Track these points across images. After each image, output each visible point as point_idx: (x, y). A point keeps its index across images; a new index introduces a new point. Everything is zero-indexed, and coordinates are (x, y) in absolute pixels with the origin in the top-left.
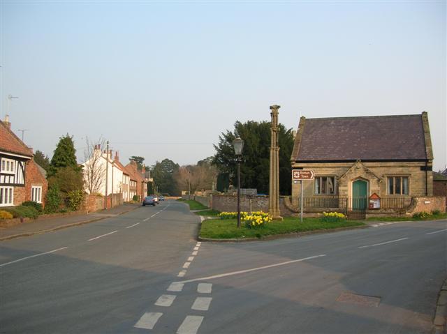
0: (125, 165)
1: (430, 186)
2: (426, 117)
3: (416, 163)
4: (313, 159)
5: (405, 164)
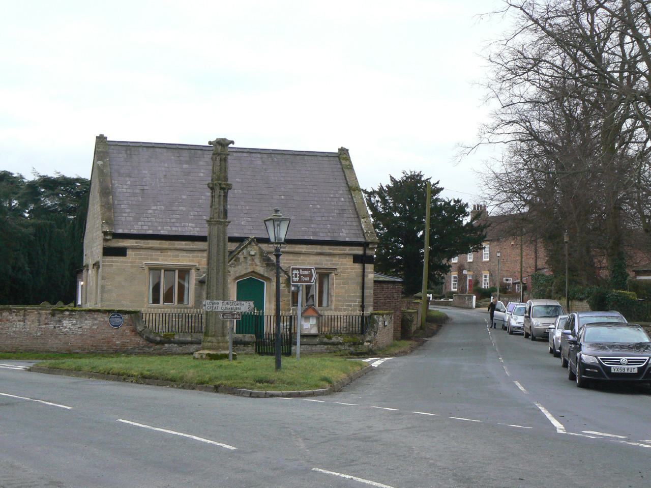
0: (127, 250)
1: (369, 292)
2: (348, 159)
3: (347, 250)
4: (150, 232)
5: (327, 249)
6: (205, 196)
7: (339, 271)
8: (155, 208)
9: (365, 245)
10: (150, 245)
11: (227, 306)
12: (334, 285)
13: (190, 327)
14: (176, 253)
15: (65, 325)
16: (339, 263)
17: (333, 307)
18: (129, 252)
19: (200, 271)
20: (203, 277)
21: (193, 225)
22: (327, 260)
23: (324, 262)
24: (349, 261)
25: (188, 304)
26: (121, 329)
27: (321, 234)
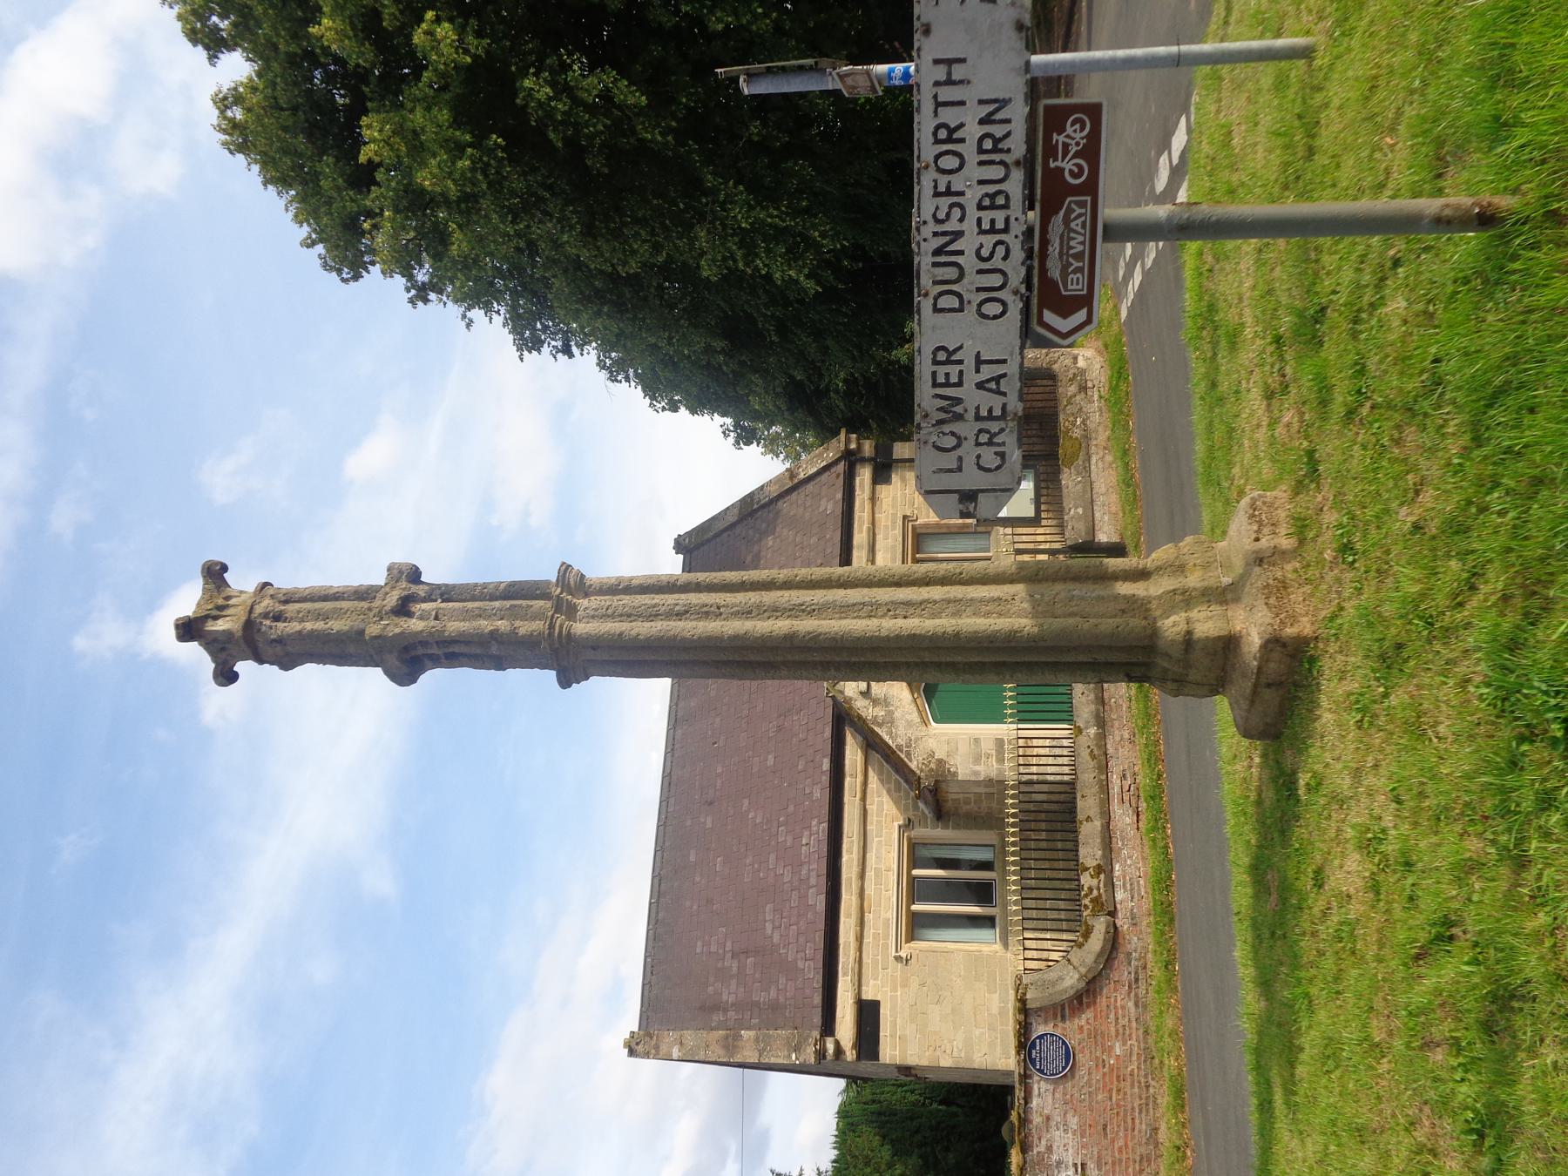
0: (864, 997)
6: (748, 811)
8: (769, 926)
10: (852, 939)
11: (968, 261)
13: (1051, 845)
18: (868, 995)
19: (912, 818)
20: (926, 812)
21: (806, 833)
24: (884, 491)
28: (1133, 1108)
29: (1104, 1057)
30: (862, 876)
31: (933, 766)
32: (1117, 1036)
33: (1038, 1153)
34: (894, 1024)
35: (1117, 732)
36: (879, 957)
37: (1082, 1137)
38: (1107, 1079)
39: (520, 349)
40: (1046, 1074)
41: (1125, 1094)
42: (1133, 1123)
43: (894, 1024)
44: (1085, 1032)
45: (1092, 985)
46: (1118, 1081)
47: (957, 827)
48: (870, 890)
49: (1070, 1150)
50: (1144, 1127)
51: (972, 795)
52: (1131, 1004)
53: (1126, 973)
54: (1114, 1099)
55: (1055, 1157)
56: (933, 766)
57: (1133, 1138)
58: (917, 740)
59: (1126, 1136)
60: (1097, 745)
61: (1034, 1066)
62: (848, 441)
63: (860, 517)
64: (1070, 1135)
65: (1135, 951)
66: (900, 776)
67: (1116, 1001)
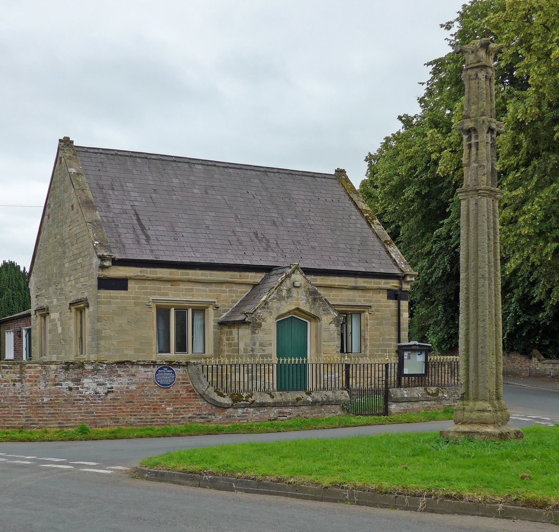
0: (129, 282)
3: (383, 283)
5: (361, 282)
7: (373, 309)
9: (401, 278)
10: (159, 275)
12: (369, 327)
14: (190, 286)
15: (85, 385)
16: (373, 299)
17: (368, 353)
18: (131, 284)
19: (219, 309)
20: (222, 317)
22: (360, 296)
23: (358, 299)
25: (204, 352)
26: (173, 389)
27: (354, 264)
28: (141, 415)
29: (165, 402)
30: (190, 281)
31: (258, 321)
32: (175, 408)
33: (117, 371)
34: (117, 298)
35: (309, 411)
36: (149, 290)
37: (126, 391)
38: (155, 404)
39: (435, 62)
40: (156, 375)
41: (148, 412)
42: (134, 415)
43: (117, 298)
44: (176, 393)
45: (199, 396)
46: (154, 409)
47: (215, 333)
48: (182, 286)
49: (119, 386)
50: (133, 420)
51: (236, 341)
52: (190, 415)
53: (205, 413)
54: (145, 406)
55: (115, 378)
56: (258, 321)
57: (127, 415)
58: (270, 312)
59: (128, 412)
60: (304, 401)
61: (160, 369)
62: (411, 276)
63: (371, 282)
64: (126, 386)
65: (215, 417)
66: (240, 302)
67: (192, 408)
